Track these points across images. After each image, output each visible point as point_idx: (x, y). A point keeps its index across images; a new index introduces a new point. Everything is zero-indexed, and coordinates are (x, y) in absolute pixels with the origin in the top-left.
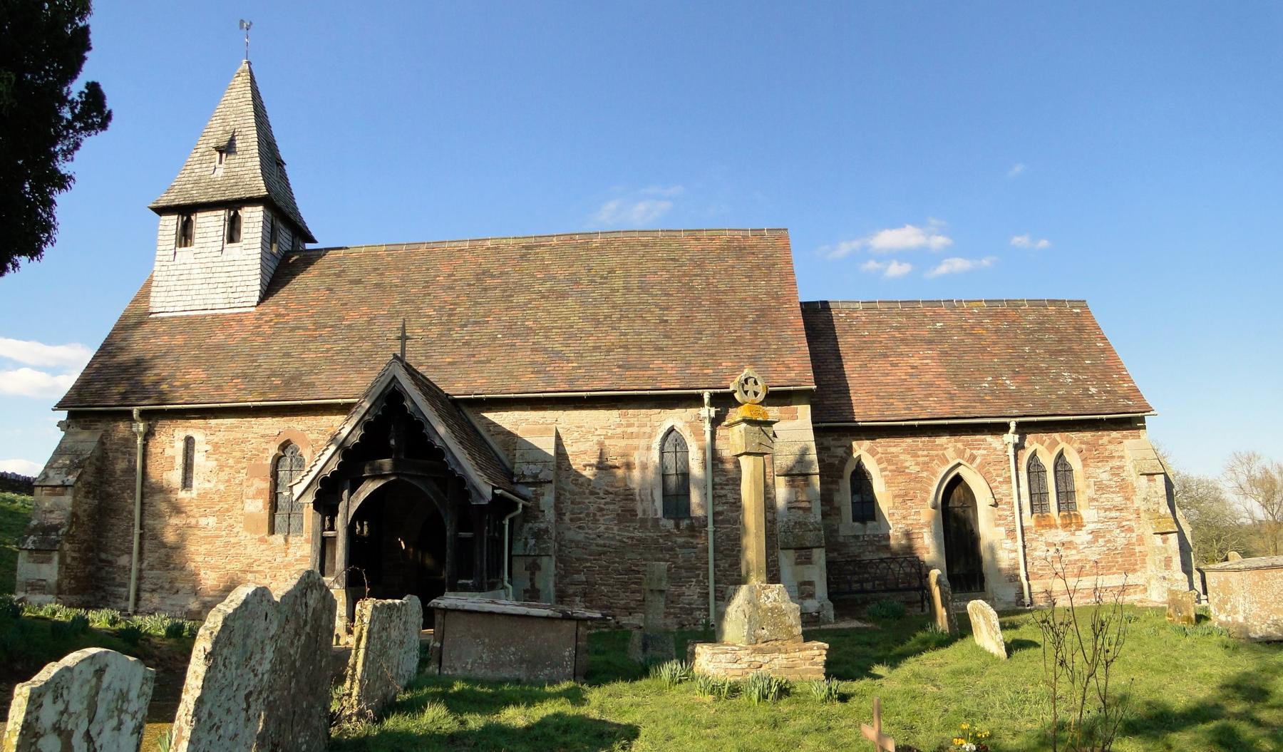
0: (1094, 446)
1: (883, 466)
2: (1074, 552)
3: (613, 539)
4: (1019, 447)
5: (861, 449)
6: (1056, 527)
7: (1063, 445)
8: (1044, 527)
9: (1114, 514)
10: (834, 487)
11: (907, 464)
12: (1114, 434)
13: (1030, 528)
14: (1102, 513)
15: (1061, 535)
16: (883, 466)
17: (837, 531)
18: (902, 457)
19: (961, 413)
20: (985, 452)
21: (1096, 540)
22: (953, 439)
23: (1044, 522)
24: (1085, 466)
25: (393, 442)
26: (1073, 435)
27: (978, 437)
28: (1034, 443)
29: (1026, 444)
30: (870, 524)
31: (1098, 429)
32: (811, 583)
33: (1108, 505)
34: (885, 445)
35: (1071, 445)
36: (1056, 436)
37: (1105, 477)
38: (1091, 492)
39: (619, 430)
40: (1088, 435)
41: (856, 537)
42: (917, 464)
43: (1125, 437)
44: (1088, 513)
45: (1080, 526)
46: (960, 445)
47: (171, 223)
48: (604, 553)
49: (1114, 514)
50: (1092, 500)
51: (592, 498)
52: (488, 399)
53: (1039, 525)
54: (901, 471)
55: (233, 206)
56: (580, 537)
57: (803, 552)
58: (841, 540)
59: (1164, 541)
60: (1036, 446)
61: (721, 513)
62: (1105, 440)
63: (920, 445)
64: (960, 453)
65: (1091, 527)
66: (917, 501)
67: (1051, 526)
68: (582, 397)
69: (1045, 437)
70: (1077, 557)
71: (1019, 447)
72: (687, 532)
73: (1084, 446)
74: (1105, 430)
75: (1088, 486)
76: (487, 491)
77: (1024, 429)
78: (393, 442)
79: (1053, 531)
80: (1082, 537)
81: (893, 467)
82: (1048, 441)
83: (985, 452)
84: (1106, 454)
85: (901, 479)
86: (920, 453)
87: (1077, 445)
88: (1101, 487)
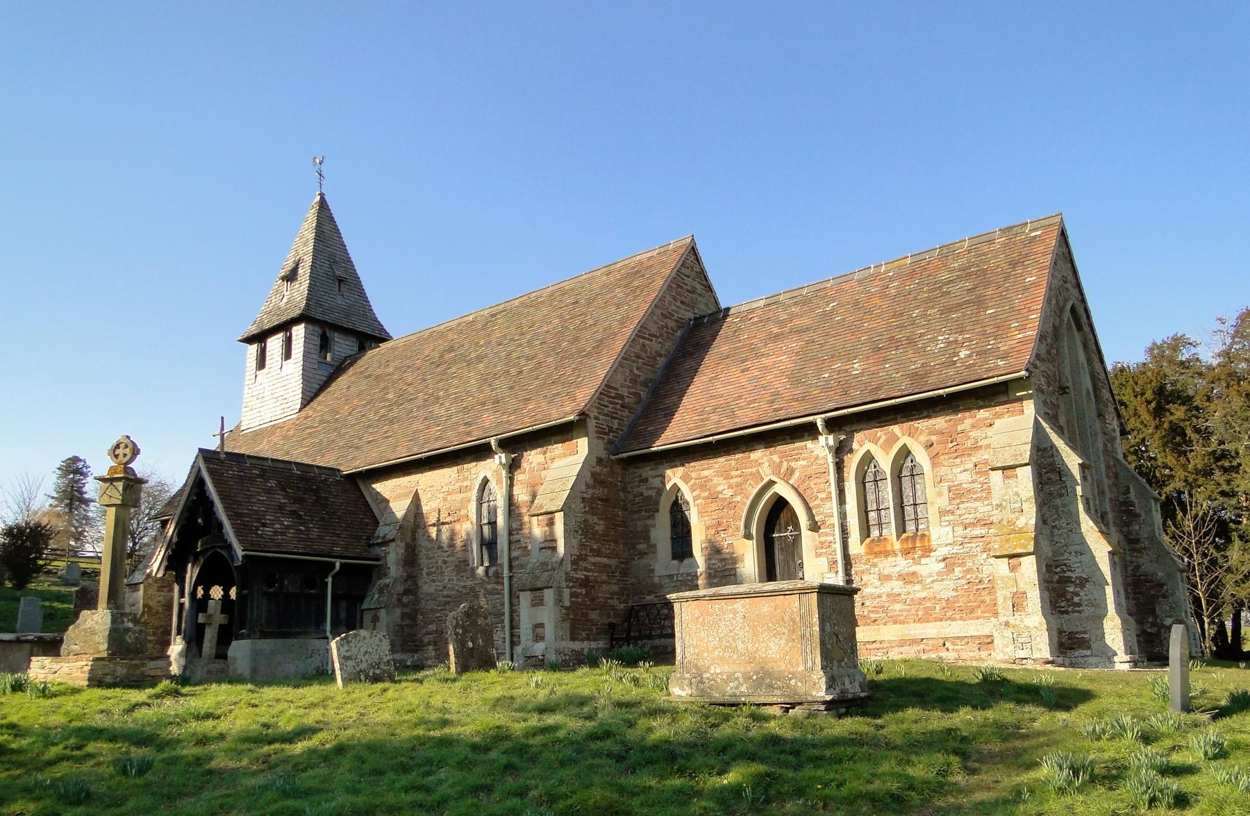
0: (951, 436)
1: (696, 493)
2: (918, 587)
3: (453, 589)
4: (840, 451)
5: (674, 476)
6: (895, 555)
7: (905, 440)
8: (877, 554)
9: (978, 531)
10: (649, 522)
11: (720, 488)
12: (983, 414)
13: (859, 556)
14: (960, 530)
15: (902, 564)
16: (696, 493)
17: (653, 571)
18: (716, 480)
19: (782, 414)
20: (804, 463)
21: (950, 568)
22: (768, 451)
23: (879, 550)
24: (934, 465)
25: (200, 521)
26: (922, 424)
27: (797, 445)
28: (864, 442)
29: (855, 446)
30: (686, 561)
31: (956, 410)
32: (541, 625)
33: (970, 518)
34: (709, 469)
35: (915, 436)
36: (896, 429)
37: (965, 478)
38: (943, 502)
39: (458, 485)
40: (940, 422)
41: (671, 577)
42: (730, 487)
43: (999, 416)
44: (940, 534)
45: (927, 551)
46: (776, 458)
47: (253, 349)
48: (448, 603)
49: (978, 531)
50: (943, 513)
51: (440, 553)
52: (367, 471)
53: (871, 552)
54: (714, 497)
55: (285, 327)
56: (432, 590)
57: (537, 593)
58: (656, 580)
59: (1013, 569)
60: (868, 446)
61: (517, 558)
62: (968, 422)
63: (733, 463)
64: (776, 468)
65: (943, 551)
66: (730, 531)
67: (887, 554)
68: (941, 396)
69: (881, 433)
70: (923, 595)
71: (840, 451)
72: (493, 579)
73: (934, 438)
74: (969, 409)
75: (940, 494)
76: (239, 552)
77: (844, 425)
78: (200, 521)
79: (890, 559)
80: (930, 567)
81: (706, 494)
82: (884, 438)
83: (804, 463)
84: (969, 444)
85: (714, 506)
86: (734, 473)
87: (923, 438)
88: (958, 494)
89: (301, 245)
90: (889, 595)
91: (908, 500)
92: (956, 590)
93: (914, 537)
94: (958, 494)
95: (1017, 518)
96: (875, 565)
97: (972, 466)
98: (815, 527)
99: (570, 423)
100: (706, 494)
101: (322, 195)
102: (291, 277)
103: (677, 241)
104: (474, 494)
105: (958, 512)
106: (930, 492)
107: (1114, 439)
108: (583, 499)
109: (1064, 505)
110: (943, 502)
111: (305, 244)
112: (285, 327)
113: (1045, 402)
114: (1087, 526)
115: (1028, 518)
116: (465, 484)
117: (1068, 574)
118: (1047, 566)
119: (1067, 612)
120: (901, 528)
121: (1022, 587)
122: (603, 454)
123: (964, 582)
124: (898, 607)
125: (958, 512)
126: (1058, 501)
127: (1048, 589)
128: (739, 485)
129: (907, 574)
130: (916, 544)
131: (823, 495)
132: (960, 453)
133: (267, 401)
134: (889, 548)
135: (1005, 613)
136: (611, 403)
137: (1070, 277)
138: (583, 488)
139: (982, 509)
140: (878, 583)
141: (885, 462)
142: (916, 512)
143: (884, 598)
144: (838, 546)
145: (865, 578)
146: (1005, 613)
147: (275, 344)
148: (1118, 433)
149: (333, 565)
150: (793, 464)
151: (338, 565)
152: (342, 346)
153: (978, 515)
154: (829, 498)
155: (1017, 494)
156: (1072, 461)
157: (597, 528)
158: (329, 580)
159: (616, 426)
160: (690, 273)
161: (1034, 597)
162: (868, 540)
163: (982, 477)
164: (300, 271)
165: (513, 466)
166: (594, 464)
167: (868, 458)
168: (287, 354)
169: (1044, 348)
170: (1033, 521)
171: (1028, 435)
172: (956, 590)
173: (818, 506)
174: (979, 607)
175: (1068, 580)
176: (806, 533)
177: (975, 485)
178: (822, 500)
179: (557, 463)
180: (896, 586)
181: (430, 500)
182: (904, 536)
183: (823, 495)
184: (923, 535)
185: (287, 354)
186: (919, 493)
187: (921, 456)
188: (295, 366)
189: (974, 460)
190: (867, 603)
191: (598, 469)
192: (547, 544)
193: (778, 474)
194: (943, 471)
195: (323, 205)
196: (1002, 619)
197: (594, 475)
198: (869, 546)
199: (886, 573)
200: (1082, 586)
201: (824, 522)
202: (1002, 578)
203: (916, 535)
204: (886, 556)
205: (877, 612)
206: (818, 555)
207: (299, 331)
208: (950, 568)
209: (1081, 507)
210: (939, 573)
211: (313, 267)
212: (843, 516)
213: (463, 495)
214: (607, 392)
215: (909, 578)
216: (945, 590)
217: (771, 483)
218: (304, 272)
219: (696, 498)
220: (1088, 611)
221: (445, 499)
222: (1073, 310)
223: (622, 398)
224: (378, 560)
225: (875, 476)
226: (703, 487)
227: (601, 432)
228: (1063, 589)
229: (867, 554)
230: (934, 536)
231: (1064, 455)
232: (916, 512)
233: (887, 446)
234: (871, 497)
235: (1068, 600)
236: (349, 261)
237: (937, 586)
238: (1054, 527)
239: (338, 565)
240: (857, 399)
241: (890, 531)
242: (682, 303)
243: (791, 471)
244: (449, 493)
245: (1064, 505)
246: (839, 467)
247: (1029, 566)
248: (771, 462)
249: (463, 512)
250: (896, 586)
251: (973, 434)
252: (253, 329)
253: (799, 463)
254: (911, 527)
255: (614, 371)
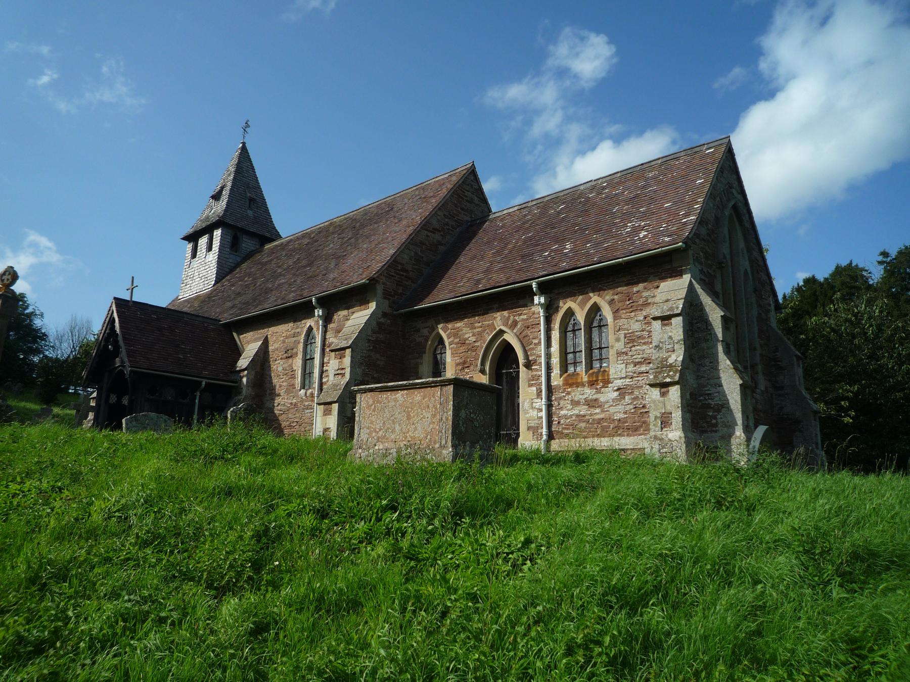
1: (451, 340)
2: (598, 410)
6: (583, 386)
8: (571, 385)
10: (419, 360)
11: (467, 336)
13: (558, 387)
14: (631, 368)
16: (451, 340)
20: (525, 317)
21: (622, 396)
23: (572, 382)
24: (615, 318)
33: (638, 358)
37: (636, 326)
38: (620, 346)
44: (617, 369)
45: (607, 382)
47: (190, 246)
50: (619, 354)
55: (208, 230)
59: (663, 395)
65: (619, 383)
66: (472, 368)
70: (602, 416)
75: (618, 340)
80: (609, 395)
81: (457, 340)
83: (525, 317)
84: (641, 301)
85: (462, 349)
86: (477, 325)
87: (608, 298)
88: (632, 340)
89: (222, 173)
90: (577, 416)
91: (596, 345)
92: (625, 413)
93: (597, 374)
94: (632, 340)
95: (670, 356)
96: (569, 393)
97: (642, 318)
98: (528, 365)
99: (364, 285)
100: (457, 340)
101: (244, 143)
102: (216, 197)
103: (461, 164)
104: (302, 338)
105: (630, 354)
106: (611, 338)
107: (768, 311)
108: (369, 341)
109: (708, 348)
110: (620, 346)
111: (229, 175)
112: (208, 230)
113: (701, 271)
114: (725, 363)
115: (677, 357)
116: (297, 331)
117: (710, 401)
118: (691, 394)
119: (706, 432)
120: (589, 366)
121: (669, 409)
122: (388, 310)
123: (632, 407)
124: (583, 425)
125: (630, 354)
126: (704, 345)
127: (690, 412)
128: (480, 334)
129: (591, 400)
130: (600, 379)
131: (536, 341)
132: (635, 308)
133: (193, 277)
134: (579, 380)
135: (655, 430)
136: (397, 274)
137: (736, 185)
138: (370, 333)
139: (648, 351)
140: (569, 407)
141: (581, 317)
142: (601, 354)
143: (574, 418)
144: (543, 379)
145: (562, 402)
146: (655, 430)
147: (203, 241)
148: (773, 307)
149: (201, 382)
150: (517, 318)
151: (204, 383)
152: (247, 244)
153: (645, 356)
154: (540, 343)
155: (670, 337)
156: (715, 315)
157: (379, 362)
158: (198, 394)
159: (400, 291)
160: (468, 188)
161: (677, 416)
162: (566, 375)
163: (649, 328)
164: (224, 193)
165: (327, 319)
166: (380, 316)
167: (570, 313)
168: (210, 248)
169: (703, 231)
170: (681, 358)
171: (683, 293)
172: (625, 413)
173: (533, 349)
174: (641, 426)
175: (709, 406)
176: (522, 369)
177: (644, 333)
178: (535, 344)
179: (355, 315)
180: (583, 410)
181: (275, 342)
182: (591, 371)
183: (536, 341)
184: (605, 371)
185: (210, 248)
186: (604, 339)
187: (607, 312)
188: (212, 258)
189: (644, 313)
190: (562, 421)
191: (382, 320)
192: (339, 372)
193: (506, 325)
194: (621, 322)
195: (244, 149)
196: (652, 433)
197: (379, 324)
198: (565, 380)
199: (576, 399)
200: (719, 411)
201: (535, 361)
202: (654, 402)
203: (599, 371)
204: (577, 387)
205: (568, 429)
206: (531, 385)
207: (218, 233)
208: (622, 396)
209: (720, 348)
210: (613, 400)
211: (231, 190)
212: (548, 356)
213: (295, 339)
214: (394, 264)
215: (592, 403)
216: (618, 412)
217: (501, 332)
218: (226, 193)
219: (450, 344)
220: (723, 431)
221: (284, 342)
222: (735, 207)
223: (407, 271)
224: (236, 382)
225: (574, 326)
226: (456, 335)
227: (387, 295)
228: (703, 414)
229: (564, 384)
230: (612, 371)
231: (707, 309)
232: (601, 354)
233: (582, 305)
234: (570, 343)
235: (707, 422)
236: (259, 188)
237: (612, 410)
238: (700, 365)
239: (204, 383)
240: (565, 268)
241: (581, 369)
242: (462, 209)
243: (515, 323)
244: (287, 337)
245: (708, 348)
246: (548, 321)
247: (675, 393)
248: (503, 317)
249: (295, 350)
250: (583, 410)
251: (645, 294)
252: (188, 230)
253: (522, 317)
254: (596, 365)
255: (400, 251)
